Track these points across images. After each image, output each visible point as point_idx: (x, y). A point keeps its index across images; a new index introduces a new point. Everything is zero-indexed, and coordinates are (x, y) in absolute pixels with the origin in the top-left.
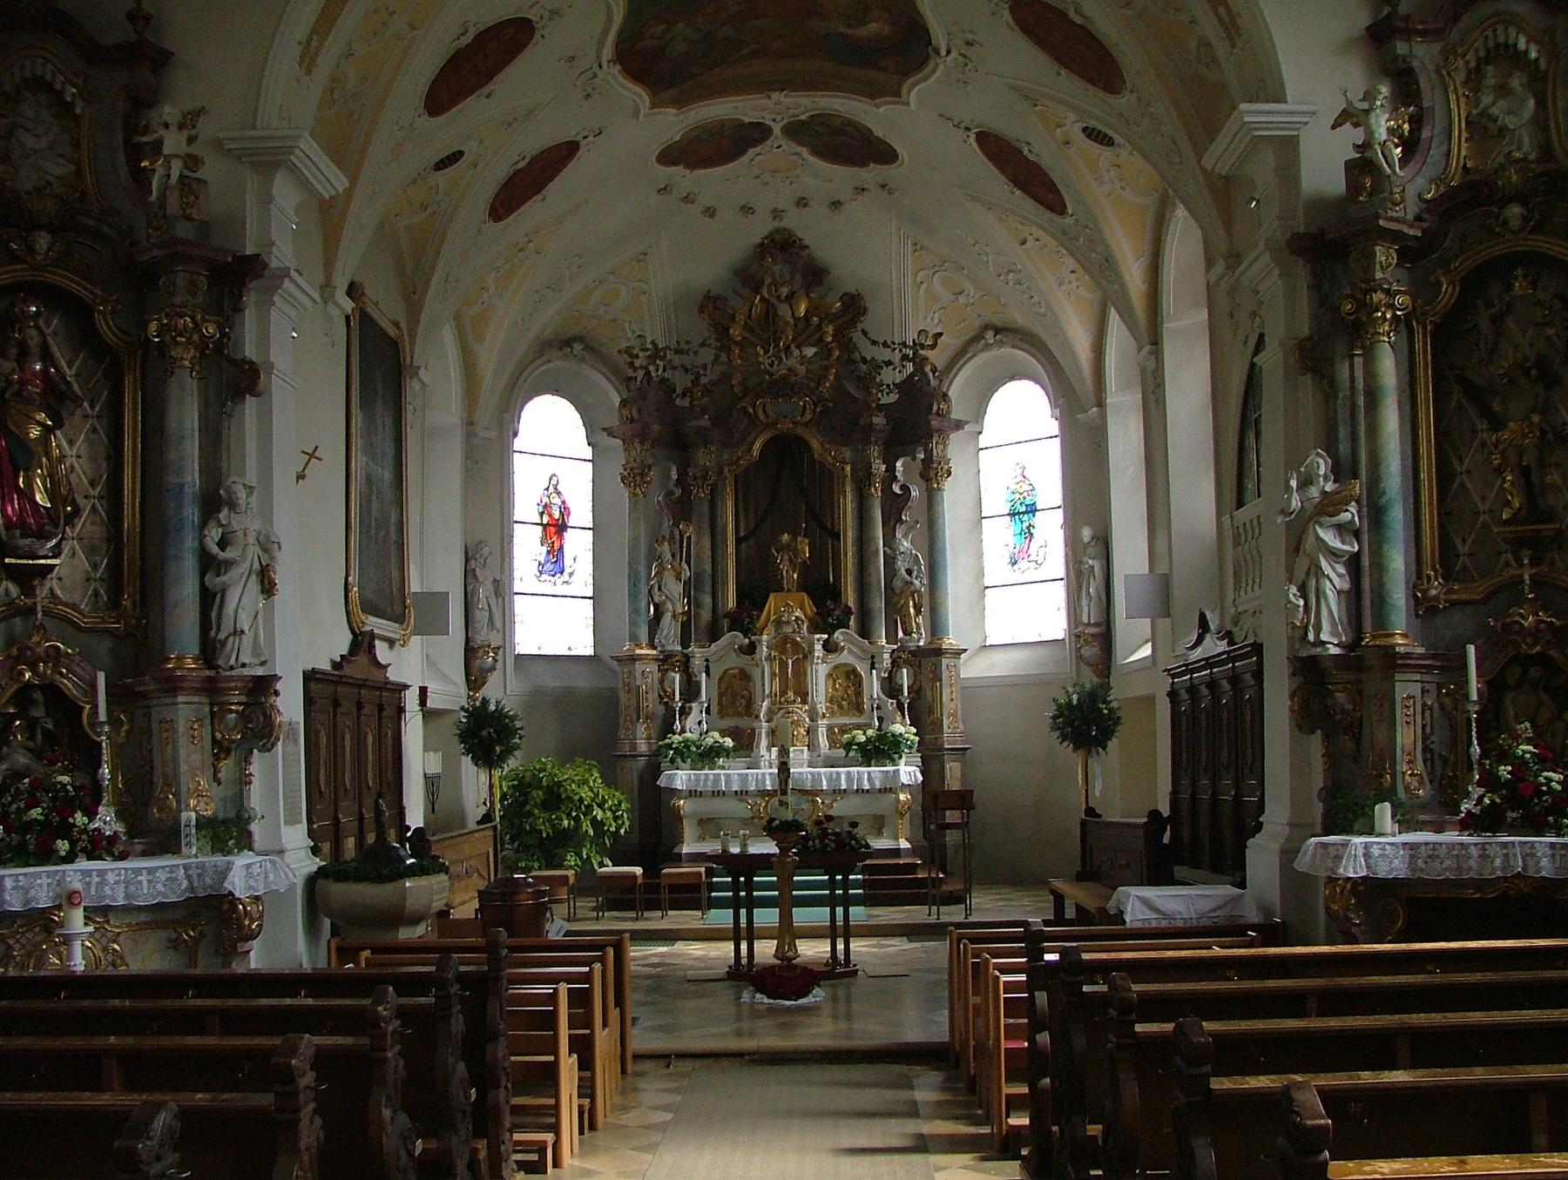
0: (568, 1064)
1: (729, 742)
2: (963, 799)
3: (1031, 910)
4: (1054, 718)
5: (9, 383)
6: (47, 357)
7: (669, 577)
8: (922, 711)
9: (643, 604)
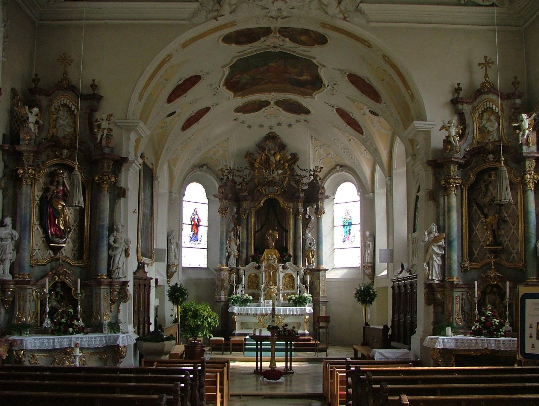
0: (219, 395)
1: (251, 298)
2: (327, 319)
3: (347, 354)
4: (356, 294)
5: (54, 193)
6: (64, 185)
7: (233, 243)
8: (313, 289)
9: (225, 252)
